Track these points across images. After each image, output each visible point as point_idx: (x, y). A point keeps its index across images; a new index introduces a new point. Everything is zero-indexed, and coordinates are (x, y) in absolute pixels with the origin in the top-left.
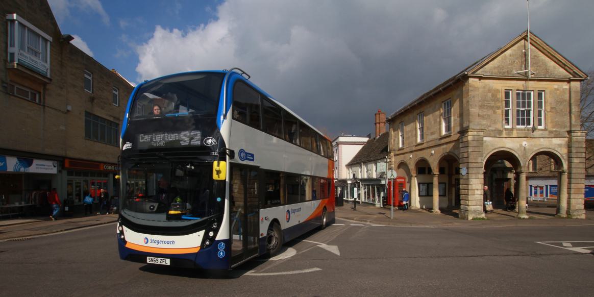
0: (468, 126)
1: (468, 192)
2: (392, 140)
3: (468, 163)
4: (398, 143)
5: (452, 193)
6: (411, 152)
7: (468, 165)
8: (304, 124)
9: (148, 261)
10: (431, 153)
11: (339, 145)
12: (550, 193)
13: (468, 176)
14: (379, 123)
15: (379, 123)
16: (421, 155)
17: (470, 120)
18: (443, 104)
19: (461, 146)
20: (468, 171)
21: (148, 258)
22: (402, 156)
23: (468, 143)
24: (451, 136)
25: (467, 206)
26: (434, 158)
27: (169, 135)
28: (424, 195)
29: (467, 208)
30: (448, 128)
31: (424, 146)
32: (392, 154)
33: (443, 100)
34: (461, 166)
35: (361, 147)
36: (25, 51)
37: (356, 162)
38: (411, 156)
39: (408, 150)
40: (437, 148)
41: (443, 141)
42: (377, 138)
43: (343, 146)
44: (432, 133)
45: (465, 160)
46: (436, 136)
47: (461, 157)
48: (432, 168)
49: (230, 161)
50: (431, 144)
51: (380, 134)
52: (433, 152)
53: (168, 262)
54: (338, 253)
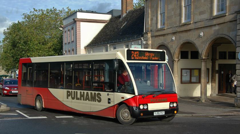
2: (150, 20)
4: (157, 23)
5: (215, 80)
6: (174, 33)
9: (154, 115)
10: (199, 35)
11: (77, 22)
12: (66, 70)
16: (185, 37)
21: (154, 113)
22: (162, 38)
24: (226, 16)
26: (202, 42)
31: (192, 26)
32: (149, 35)
35: (101, 26)
37: (97, 43)
38: (174, 38)
39: (170, 31)
40: (207, 30)
41: (215, 22)
42: (124, 16)
43: (82, 23)
44: (201, 13)
46: (206, 16)
49: (150, 47)
50: (199, 25)
51: (127, 12)
52: (202, 34)
53: (163, 113)
54: (47, 118)
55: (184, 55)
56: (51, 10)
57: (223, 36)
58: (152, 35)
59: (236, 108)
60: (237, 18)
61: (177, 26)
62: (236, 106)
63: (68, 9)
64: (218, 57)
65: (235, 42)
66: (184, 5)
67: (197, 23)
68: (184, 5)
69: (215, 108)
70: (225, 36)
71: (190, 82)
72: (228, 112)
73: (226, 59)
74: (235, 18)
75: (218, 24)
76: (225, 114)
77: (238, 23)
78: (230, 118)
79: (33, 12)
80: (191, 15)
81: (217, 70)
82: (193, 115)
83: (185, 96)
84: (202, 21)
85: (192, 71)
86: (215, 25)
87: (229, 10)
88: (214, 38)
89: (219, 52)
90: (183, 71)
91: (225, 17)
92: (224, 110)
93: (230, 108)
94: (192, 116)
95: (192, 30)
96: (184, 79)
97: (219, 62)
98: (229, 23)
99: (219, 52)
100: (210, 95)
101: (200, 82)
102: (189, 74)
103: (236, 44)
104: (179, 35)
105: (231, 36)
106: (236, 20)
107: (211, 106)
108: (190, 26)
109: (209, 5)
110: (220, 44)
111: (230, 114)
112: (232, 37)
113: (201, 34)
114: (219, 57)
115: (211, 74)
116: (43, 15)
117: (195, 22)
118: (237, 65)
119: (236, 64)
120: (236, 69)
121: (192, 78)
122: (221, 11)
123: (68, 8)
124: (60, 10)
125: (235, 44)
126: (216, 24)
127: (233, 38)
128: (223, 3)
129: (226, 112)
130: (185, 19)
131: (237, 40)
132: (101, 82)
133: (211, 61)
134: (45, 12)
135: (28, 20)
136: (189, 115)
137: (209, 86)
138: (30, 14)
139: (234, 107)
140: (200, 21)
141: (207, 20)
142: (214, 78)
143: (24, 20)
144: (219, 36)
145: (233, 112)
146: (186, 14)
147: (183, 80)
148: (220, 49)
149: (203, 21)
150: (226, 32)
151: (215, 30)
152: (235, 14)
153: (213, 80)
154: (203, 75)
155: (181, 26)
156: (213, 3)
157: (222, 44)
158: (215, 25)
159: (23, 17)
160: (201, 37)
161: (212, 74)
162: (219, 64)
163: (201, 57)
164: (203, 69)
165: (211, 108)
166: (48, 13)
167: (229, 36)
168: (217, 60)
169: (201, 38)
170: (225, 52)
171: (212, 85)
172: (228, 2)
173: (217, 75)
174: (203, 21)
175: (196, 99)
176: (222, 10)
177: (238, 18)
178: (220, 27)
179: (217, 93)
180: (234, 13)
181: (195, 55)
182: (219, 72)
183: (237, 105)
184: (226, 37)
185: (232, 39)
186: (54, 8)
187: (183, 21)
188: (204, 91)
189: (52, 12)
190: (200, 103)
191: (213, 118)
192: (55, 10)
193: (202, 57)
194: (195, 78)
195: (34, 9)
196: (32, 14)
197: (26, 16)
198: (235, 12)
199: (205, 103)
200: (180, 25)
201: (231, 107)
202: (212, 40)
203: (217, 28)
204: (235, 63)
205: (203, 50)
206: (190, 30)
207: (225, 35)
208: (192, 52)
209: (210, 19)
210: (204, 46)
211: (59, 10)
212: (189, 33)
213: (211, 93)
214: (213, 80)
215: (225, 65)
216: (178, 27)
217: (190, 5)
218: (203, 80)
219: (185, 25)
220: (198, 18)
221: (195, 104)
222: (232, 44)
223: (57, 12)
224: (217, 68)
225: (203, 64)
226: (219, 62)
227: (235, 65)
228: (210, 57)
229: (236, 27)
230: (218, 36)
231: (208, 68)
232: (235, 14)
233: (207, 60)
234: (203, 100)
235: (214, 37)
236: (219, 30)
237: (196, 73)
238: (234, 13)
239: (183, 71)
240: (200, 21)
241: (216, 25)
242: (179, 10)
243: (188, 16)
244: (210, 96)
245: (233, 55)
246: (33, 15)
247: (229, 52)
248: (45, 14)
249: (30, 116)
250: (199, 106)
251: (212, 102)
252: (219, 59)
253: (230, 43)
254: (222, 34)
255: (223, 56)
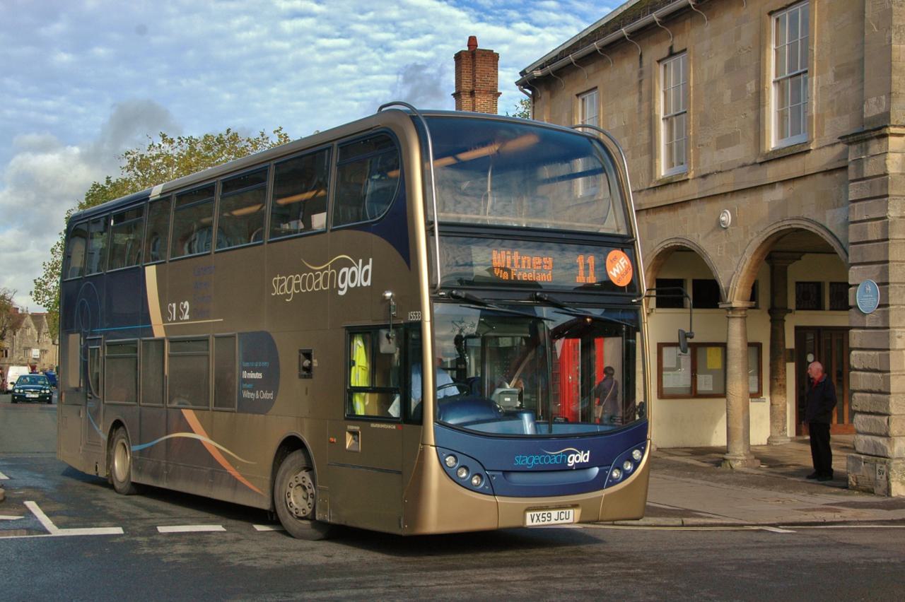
0: (887, 116)
1: (887, 382)
3: (887, 262)
5: (784, 387)
7: (885, 272)
8: (587, 500)
10: (719, 222)
13: (886, 316)
14: (472, 94)
15: (472, 94)
17: (895, 87)
18: (580, 100)
19: (852, 196)
20: (885, 295)
23: (885, 184)
24: (808, 151)
25: (881, 440)
27: (524, 259)
28: (665, 385)
29: (883, 448)
30: (794, 115)
31: (690, 190)
33: (578, 92)
34: (854, 275)
36: (262, 231)
40: (744, 202)
41: (772, 172)
44: (725, 142)
45: (873, 253)
46: (741, 152)
47: (852, 239)
48: (723, 285)
52: (726, 218)
55: (668, 295)
56: (220, 141)
57: (803, 225)
58: (640, 205)
59: (853, 495)
60: (847, 159)
61: (642, 188)
62: (852, 484)
63: (280, 136)
64: (792, 303)
65: (844, 246)
66: (662, 115)
67: (709, 178)
68: (665, 114)
69: (773, 493)
70: (806, 223)
71: (693, 393)
72: (821, 510)
73: (824, 309)
74: (839, 161)
75: (784, 182)
76: (809, 517)
77: (850, 179)
78: (825, 533)
79: (160, 146)
80: (687, 148)
81: (791, 350)
82: (685, 519)
83: (675, 446)
84: (726, 171)
85: (700, 351)
86: (772, 185)
87: (820, 132)
88: (771, 231)
89: (797, 283)
90: (665, 350)
91: (807, 156)
92: (808, 498)
93: (831, 493)
94: (683, 525)
95: (692, 203)
96: (670, 382)
97: (795, 320)
98: (819, 177)
99: (797, 283)
100: (765, 442)
101: (723, 395)
102: (686, 360)
103: (847, 255)
104: (648, 223)
105: (828, 226)
106: (845, 168)
107: (763, 486)
108: (685, 187)
109: (751, 115)
110: (797, 255)
111: (829, 516)
112: (832, 230)
113: (723, 219)
114: (797, 303)
115: (768, 360)
116: (191, 156)
117: (704, 173)
118: (851, 331)
119: (852, 328)
120: (851, 346)
121: (700, 378)
122: (792, 135)
123: (277, 131)
124: (252, 139)
125: (845, 257)
126: (775, 183)
127: (836, 234)
128: (799, 106)
129: (814, 510)
130: (670, 164)
131: (850, 241)
132: (616, 335)
133: (769, 318)
134: (199, 147)
135: (140, 173)
136: (673, 519)
137: (760, 411)
138: (147, 154)
139: (846, 487)
140: (721, 172)
141: (744, 166)
142: (781, 377)
143: (126, 175)
144: (787, 223)
145: (839, 511)
146: (670, 148)
147: (664, 386)
148: (798, 272)
149: (730, 170)
150: (811, 209)
151: (774, 201)
152: (840, 148)
153: (777, 384)
154: (736, 367)
155: (654, 188)
156: (764, 106)
157: (807, 255)
158: (772, 185)
159: (126, 163)
160: (725, 228)
161: (771, 365)
162: (797, 329)
163: (724, 302)
164: (736, 344)
165: (760, 492)
166: (209, 148)
167: (823, 226)
168: (791, 311)
169: (723, 232)
170: (818, 286)
171: (772, 404)
172: (814, 103)
173: (791, 368)
174: (730, 170)
175: (713, 455)
176: (796, 131)
177: (850, 160)
178: (791, 191)
179: (794, 435)
180: (839, 143)
181: (708, 294)
182: (799, 357)
183: (857, 483)
184: (820, 232)
185: (832, 234)
186: (228, 131)
187: (662, 171)
188: (741, 428)
189: (224, 146)
190: (723, 473)
191: (761, 537)
192: (235, 138)
193: (728, 300)
194: (710, 377)
195: (164, 136)
196: (154, 153)
197: (134, 160)
198: (839, 138)
199: (743, 473)
200: (651, 186)
201: (836, 490)
202: (763, 237)
203: (779, 194)
204: (846, 324)
205: (734, 278)
206: (686, 203)
207: (807, 220)
208: (696, 283)
209: (755, 164)
210: (735, 260)
211: (248, 140)
212: (682, 213)
213: (769, 435)
214: (777, 384)
215: (818, 330)
216: (643, 193)
217: (684, 115)
218: (737, 387)
219: (667, 184)
220: (712, 159)
221: (704, 477)
222: (836, 253)
223: (243, 146)
224: (790, 343)
225: (736, 327)
226: (795, 320)
227: (847, 329)
228: (764, 299)
229: (847, 192)
230: (785, 225)
231: (752, 339)
232: (840, 148)
233: (749, 311)
234: (735, 460)
235: (769, 229)
236: (784, 203)
237: (712, 359)
238: (839, 143)
239: (665, 350)
240: (719, 170)
241: (777, 185)
242: (645, 133)
243: (678, 154)
244: (768, 443)
245: (841, 297)
246: (158, 157)
247: (831, 284)
248: (200, 152)
249: (60, 526)
250: (718, 482)
251: (770, 467)
252: (797, 309)
253: (830, 251)
254: (798, 219)
255: (810, 297)
